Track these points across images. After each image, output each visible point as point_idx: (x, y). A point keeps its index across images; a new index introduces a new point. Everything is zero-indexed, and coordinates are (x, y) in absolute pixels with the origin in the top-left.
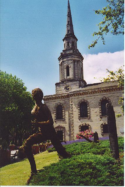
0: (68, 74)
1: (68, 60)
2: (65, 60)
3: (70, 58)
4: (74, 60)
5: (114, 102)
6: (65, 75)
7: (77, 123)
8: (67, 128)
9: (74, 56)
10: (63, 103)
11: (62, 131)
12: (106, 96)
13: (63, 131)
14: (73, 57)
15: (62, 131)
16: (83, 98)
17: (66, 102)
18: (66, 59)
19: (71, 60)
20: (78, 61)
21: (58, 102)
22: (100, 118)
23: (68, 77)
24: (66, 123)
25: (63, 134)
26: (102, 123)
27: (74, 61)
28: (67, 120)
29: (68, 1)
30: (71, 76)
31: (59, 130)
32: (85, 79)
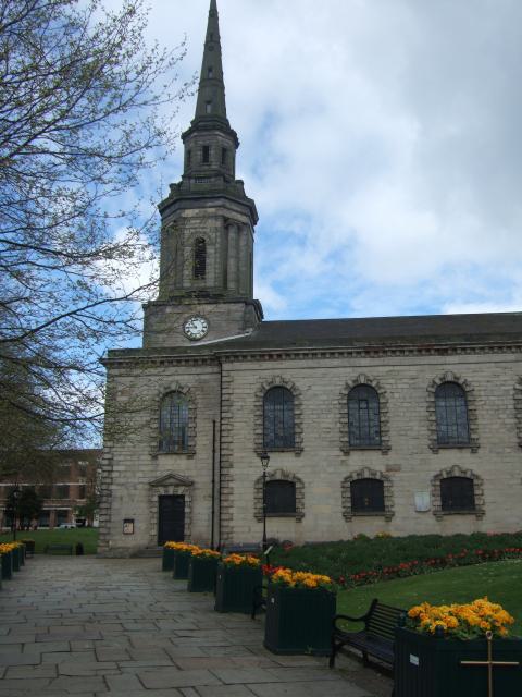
0: (199, 270)
1: (205, 217)
2: (189, 213)
3: (213, 210)
4: (226, 219)
5: (396, 395)
6: (188, 272)
7: (246, 472)
8: (203, 479)
9: (228, 204)
10: (190, 385)
11: (183, 496)
12: (372, 373)
13: (187, 499)
14: (224, 206)
15: (183, 496)
16: (278, 372)
17: (206, 381)
18: (197, 211)
19: (216, 217)
20: (240, 227)
21: (170, 379)
22: (342, 453)
24: (191, 455)
25: (187, 510)
27: (227, 223)
29: (213, 15)
30: (211, 279)
31: (171, 493)
32: (260, 293)
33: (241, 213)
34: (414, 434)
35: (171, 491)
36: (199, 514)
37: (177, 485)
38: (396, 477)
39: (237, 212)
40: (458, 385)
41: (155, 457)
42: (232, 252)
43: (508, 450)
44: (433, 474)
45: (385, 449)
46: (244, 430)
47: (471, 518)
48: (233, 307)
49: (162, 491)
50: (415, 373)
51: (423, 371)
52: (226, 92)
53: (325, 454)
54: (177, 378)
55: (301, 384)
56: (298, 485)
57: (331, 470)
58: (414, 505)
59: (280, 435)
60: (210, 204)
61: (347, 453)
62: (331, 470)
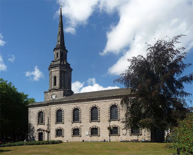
0: (55, 84)
2: (53, 70)
3: (58, 69)
6: (53, 84)
20: (65, 72)
23: (55, 87)
26: (72, 128)
28: (46, 122)
33: (64, 69)
34: (86, 118)
35: (40, 132)
36: (46, 135)
37: (41, 131)
38: (82, 128)
39: (63, 69)
40: (94, 107)
41: (38, 125)
42: (63, 79)
43: (106, 121)
44: (90, 127)
45: (109, 128)
46: (53, 118)
47: (79, 137)
48: (61, 92)
49: (39, 132)
50: (87, 105)
51: (89, 105)
52: (64, 38)
53: (68, 123)
54: (41, 109)
55: (64, 109)
56: (63, 130)
57: (69, 127)
58: (85, 134)
59: (59, 118)
60: (57, 68)
61: (73, 123)
62: (69, 127)
